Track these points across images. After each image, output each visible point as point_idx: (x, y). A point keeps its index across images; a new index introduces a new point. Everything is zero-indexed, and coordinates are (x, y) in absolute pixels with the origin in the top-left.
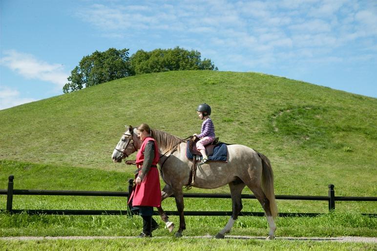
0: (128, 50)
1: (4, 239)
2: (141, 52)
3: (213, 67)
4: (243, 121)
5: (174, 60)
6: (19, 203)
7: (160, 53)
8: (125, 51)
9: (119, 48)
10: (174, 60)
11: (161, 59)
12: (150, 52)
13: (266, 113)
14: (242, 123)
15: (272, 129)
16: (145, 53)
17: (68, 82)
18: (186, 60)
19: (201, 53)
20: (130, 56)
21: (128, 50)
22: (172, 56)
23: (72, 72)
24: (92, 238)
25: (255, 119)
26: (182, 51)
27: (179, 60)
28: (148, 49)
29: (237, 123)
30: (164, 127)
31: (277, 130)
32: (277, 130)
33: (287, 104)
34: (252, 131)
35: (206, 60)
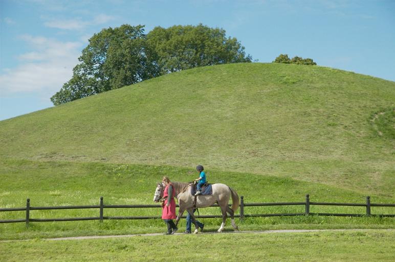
0: (144, 26)
1: (2, 241)
2: (158, 31)
3: (239, 45)
4: (347, 125)
5: (199, 40)
6: (374, 210)
7: (182, 31)
8: (140, 26)
9: (134, 24)
10: (199, 40)
11: (187, 38)
12: (169, 29)
13: (363, 116)
14: (346, 127)
15: (375, 133)
16: (164, 30)
17: (80, 63)
18: (212, 39)
19: (226, 31)
20: (146, 32)
21: (144, 26)
22: (196, 34)
23: (84, 51)
24: (11, 241)
25: (355, 122)
26: (206, 28)
27: (204, 40)
28: (166, 26)
29: (341, 126)
30: (276, 131)
31: (381, 134)
32: (381, 134)
33: (377, 106)
34: (358, 134)
35: (232, 38)
